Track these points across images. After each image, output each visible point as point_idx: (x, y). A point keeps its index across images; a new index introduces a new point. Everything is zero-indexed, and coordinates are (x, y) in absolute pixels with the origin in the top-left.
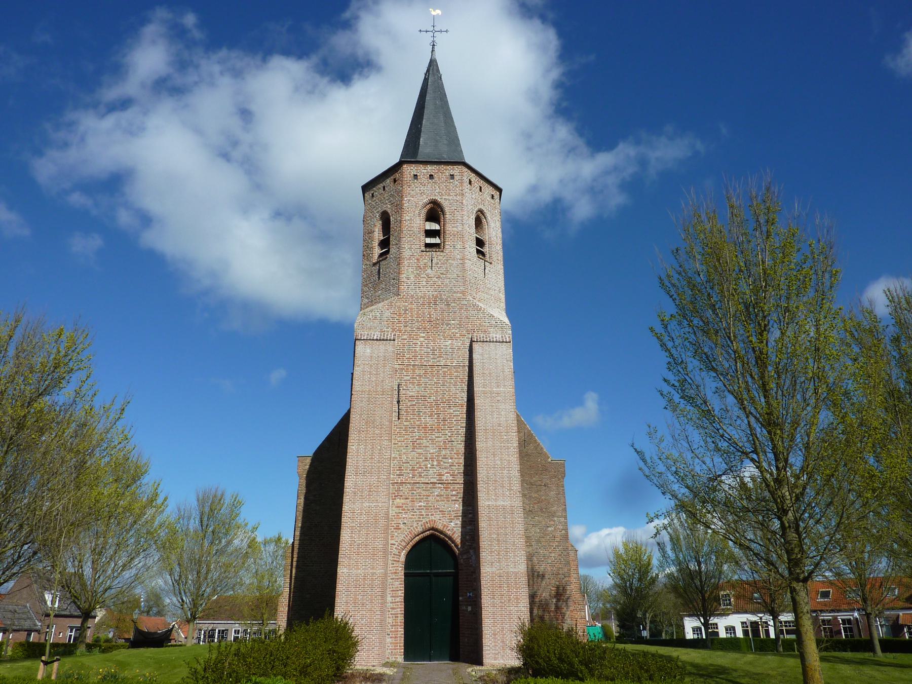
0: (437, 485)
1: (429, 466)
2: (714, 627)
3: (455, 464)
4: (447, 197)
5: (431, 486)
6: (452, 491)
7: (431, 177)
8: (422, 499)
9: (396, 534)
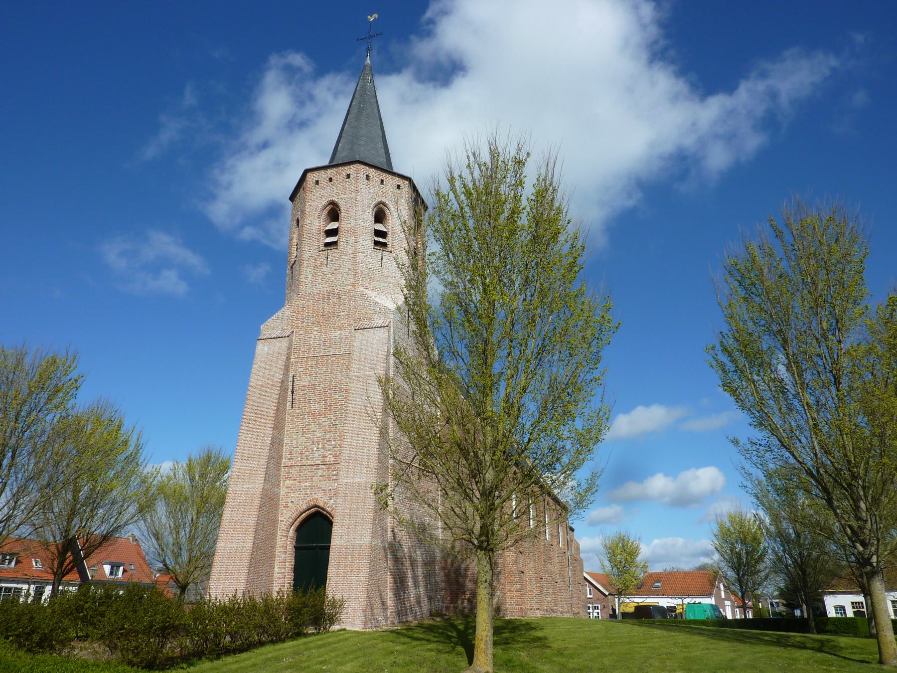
0: (321, 466)
1: (315, 449)
2: (860, 607)
3: (337, 446)
4: (343, 196)
5: (315, 467)
6: (333, 471)
7: (331, 180)
8: (308, 479)
9: (285, 512)
